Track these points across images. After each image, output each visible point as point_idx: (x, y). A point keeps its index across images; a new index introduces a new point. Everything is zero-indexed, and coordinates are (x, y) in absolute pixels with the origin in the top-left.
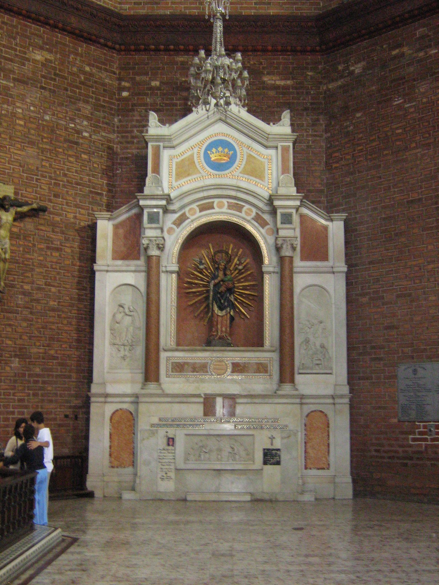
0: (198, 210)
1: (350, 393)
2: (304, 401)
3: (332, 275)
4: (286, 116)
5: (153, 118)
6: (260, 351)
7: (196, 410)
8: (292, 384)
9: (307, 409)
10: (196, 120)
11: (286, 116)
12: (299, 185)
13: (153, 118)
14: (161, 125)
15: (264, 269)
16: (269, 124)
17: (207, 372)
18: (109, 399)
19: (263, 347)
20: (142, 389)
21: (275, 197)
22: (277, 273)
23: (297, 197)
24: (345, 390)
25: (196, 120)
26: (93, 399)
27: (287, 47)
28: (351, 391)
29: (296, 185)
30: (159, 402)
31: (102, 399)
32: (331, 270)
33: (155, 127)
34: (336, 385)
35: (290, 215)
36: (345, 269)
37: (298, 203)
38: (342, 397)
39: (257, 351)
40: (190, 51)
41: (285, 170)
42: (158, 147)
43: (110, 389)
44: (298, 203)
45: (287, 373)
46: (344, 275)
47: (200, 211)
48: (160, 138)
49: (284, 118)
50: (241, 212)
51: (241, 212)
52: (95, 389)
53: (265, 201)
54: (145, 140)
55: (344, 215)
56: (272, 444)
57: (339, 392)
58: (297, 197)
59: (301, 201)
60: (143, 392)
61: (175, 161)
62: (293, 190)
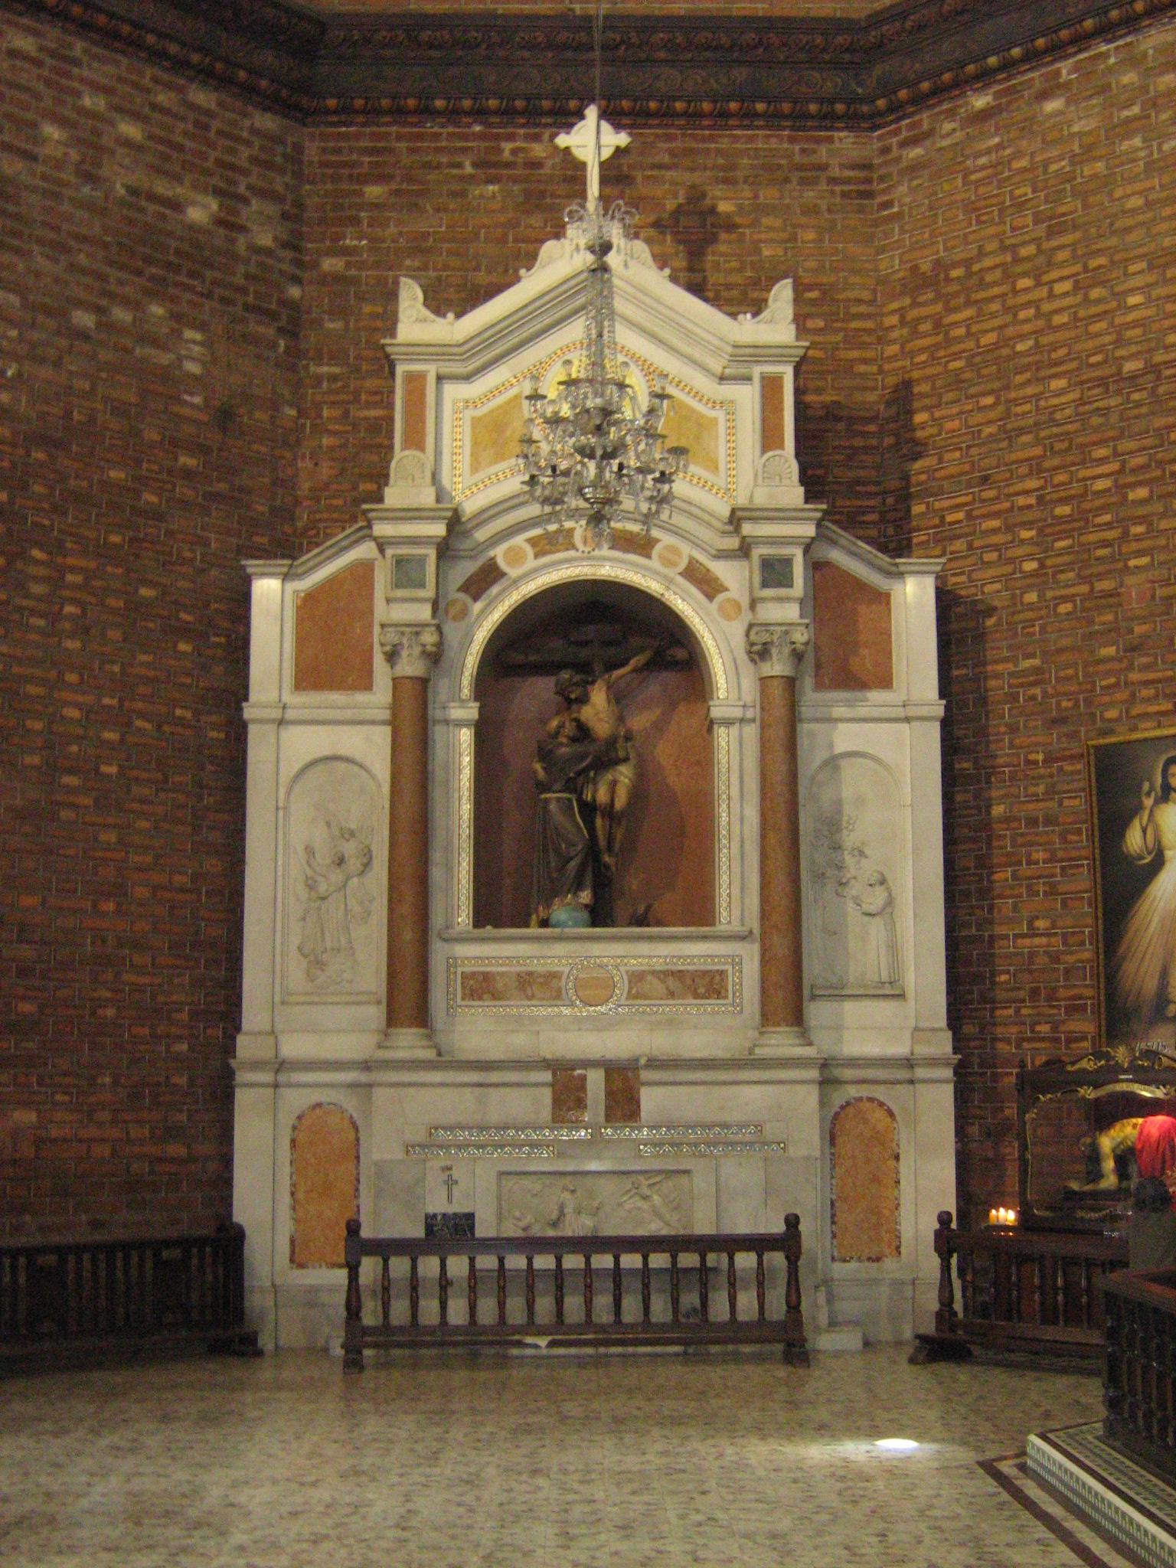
0: (529, 551)
1: (955, 1050)
2: (282, 1078)
3: (906, 726)
4: (782, 297)
5: (411, 297)
6: (705, 938)
7: (532, 1101)
8: (423, 1031)
9: (839, 1097)
10: (671, 309)
11: (782, 297)
12: (813, 484)
13: (411, 297)
14: (432, 316)
15: (716, 712)
16: (733, 315)
17: (558, 996)
18: (921, 1073)
19: (713, 924)
20: (379, 1046)
21: (380, 514)
22: (384, 723)
23: (806, 514)
24: (943, 1045)
25: (671, 309)
26: (242, 1077)
27: (379, 99)
28: (959, 1043)
29: (805, 479)
30: (424, 1085)
31: (266, 1077)
32: (900, 712)
33: (416, 323)
34: (916, 1029)
35: (788, 562)
36: (939, 710)
37: (810, 530)
38: (933, 1062)
39: (641, 938)
40: (409, 112)
41: (770, 439)
42: (421, 377)
43: (293, 1047)
44: (810, 530)
45: (789, 996)
46: (937, 725)
47: (536, 556)
48: (440, 352)
49: (775, 301)
50: (649, 557)
51: (649, 557)
52: (246, 1046)
53: (719, 525)
54: (387, 356)
55: (937, 564)
56: (450, 1200)
57: (922, 1050)
58: (806, 514)
59: (819, 525)
60: (382, 1054)
61: (470, 414)
62: (793, 494)
